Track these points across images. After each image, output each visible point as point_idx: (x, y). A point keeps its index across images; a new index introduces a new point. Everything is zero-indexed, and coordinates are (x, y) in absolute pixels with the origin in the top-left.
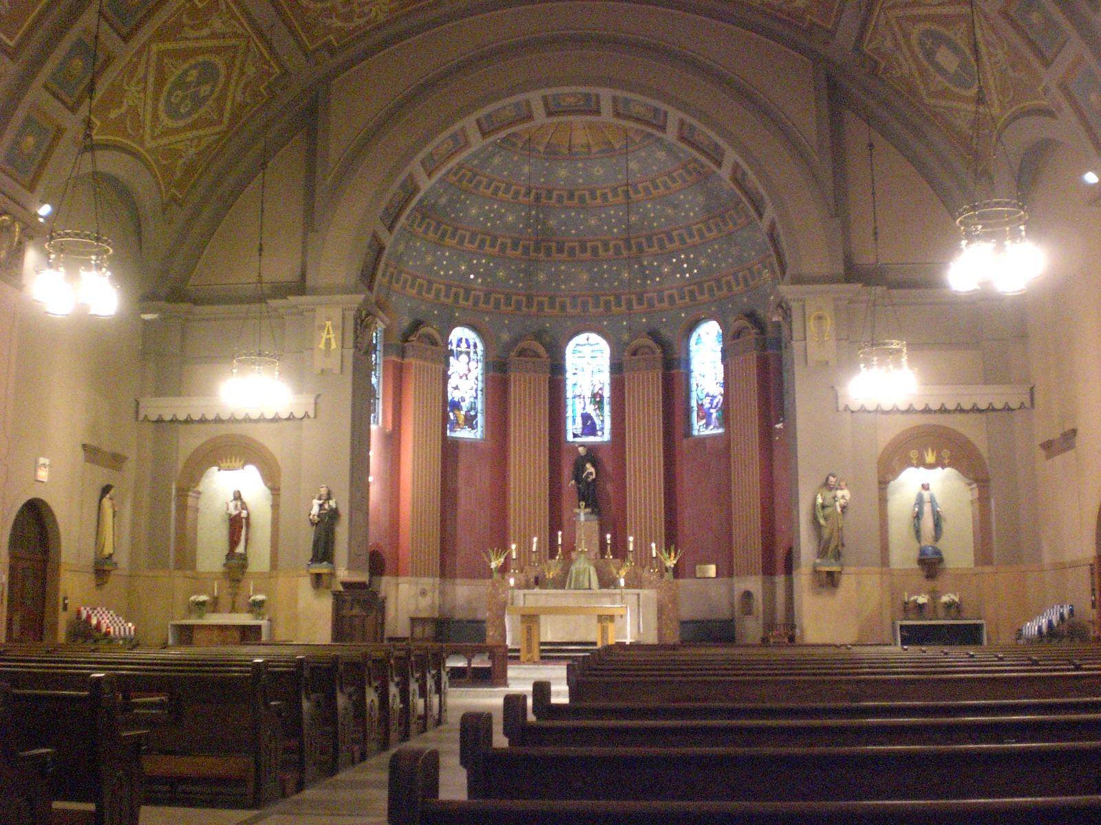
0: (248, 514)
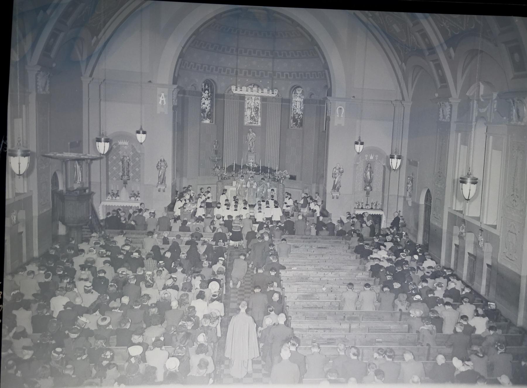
0: (139, 160)
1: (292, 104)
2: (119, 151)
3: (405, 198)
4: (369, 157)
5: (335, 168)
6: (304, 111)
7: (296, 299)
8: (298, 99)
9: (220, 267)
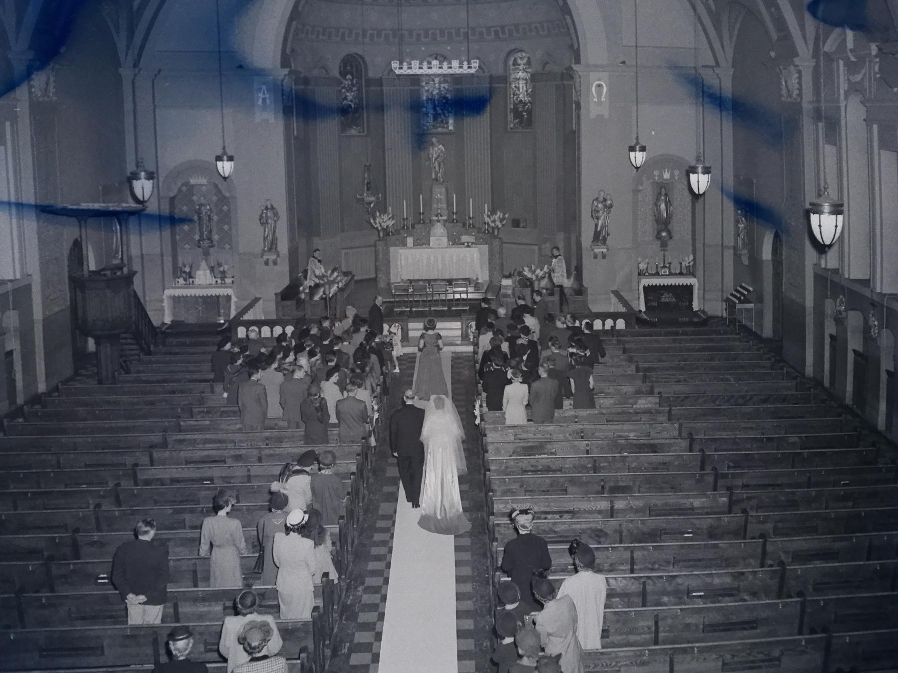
1: (510, 84)
2: (193, 195)
3: (735, 248)
4: (661, 176)
5: (597, 199)
6: (532, 95)
7: (511, 456)
8: (521, 74)
9: (365, 402)
